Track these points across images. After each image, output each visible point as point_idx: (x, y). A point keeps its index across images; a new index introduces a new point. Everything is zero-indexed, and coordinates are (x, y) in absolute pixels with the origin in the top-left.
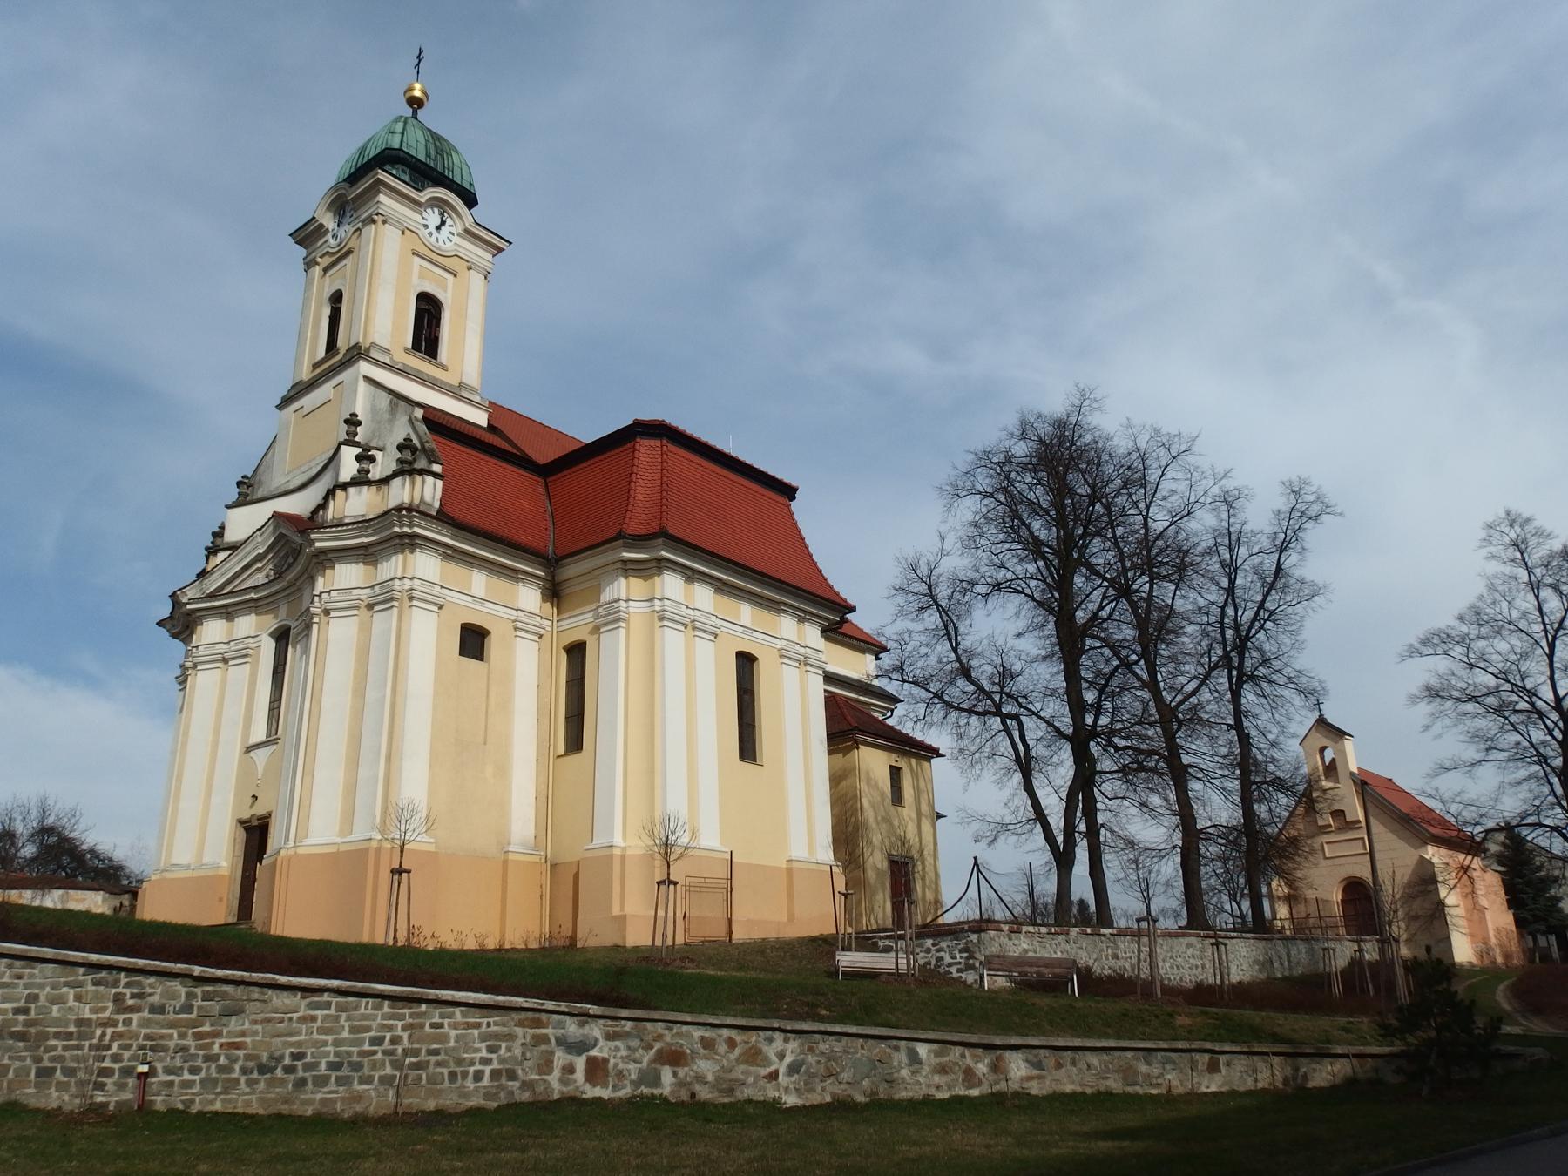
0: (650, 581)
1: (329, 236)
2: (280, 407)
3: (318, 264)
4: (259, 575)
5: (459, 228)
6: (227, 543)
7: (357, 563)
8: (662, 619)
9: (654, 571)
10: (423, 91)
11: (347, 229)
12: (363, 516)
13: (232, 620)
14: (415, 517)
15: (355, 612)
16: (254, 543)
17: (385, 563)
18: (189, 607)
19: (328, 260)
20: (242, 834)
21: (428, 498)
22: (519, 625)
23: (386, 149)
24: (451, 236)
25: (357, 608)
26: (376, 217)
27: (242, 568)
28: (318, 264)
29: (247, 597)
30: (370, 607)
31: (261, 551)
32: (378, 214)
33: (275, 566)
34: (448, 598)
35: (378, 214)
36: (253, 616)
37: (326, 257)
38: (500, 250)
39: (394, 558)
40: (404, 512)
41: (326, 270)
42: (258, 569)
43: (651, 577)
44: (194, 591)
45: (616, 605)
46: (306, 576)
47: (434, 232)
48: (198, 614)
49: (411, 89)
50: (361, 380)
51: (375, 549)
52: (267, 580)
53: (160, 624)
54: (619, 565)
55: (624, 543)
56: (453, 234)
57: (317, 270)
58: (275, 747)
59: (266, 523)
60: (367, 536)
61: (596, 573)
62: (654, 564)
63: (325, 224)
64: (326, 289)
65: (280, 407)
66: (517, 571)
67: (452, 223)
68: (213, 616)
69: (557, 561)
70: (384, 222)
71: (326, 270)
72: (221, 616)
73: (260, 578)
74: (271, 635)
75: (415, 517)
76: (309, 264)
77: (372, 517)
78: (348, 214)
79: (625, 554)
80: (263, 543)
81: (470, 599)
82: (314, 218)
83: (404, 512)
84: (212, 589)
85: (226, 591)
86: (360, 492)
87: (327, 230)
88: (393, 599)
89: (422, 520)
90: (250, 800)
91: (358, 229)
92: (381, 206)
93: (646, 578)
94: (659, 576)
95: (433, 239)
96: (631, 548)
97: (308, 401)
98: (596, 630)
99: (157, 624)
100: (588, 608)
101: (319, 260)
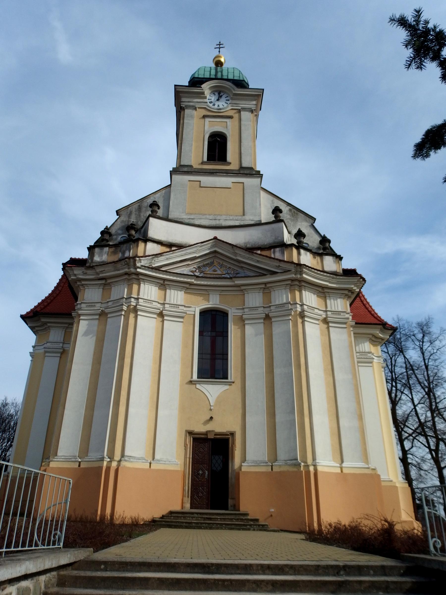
1: (207, 100)
16: (195, 249)
18: (138, 270)
20: (190, 441)
25: (318, 320)
34: (188, 313)
37: (203, 110)
41: (204, 117)
44: (146, 261)
60: (330, 282)
63: (205, 93)
72: (156, 284)
73: (185, 270)
87: (205, 98)
90: (209, 418)
95: (216, 106)
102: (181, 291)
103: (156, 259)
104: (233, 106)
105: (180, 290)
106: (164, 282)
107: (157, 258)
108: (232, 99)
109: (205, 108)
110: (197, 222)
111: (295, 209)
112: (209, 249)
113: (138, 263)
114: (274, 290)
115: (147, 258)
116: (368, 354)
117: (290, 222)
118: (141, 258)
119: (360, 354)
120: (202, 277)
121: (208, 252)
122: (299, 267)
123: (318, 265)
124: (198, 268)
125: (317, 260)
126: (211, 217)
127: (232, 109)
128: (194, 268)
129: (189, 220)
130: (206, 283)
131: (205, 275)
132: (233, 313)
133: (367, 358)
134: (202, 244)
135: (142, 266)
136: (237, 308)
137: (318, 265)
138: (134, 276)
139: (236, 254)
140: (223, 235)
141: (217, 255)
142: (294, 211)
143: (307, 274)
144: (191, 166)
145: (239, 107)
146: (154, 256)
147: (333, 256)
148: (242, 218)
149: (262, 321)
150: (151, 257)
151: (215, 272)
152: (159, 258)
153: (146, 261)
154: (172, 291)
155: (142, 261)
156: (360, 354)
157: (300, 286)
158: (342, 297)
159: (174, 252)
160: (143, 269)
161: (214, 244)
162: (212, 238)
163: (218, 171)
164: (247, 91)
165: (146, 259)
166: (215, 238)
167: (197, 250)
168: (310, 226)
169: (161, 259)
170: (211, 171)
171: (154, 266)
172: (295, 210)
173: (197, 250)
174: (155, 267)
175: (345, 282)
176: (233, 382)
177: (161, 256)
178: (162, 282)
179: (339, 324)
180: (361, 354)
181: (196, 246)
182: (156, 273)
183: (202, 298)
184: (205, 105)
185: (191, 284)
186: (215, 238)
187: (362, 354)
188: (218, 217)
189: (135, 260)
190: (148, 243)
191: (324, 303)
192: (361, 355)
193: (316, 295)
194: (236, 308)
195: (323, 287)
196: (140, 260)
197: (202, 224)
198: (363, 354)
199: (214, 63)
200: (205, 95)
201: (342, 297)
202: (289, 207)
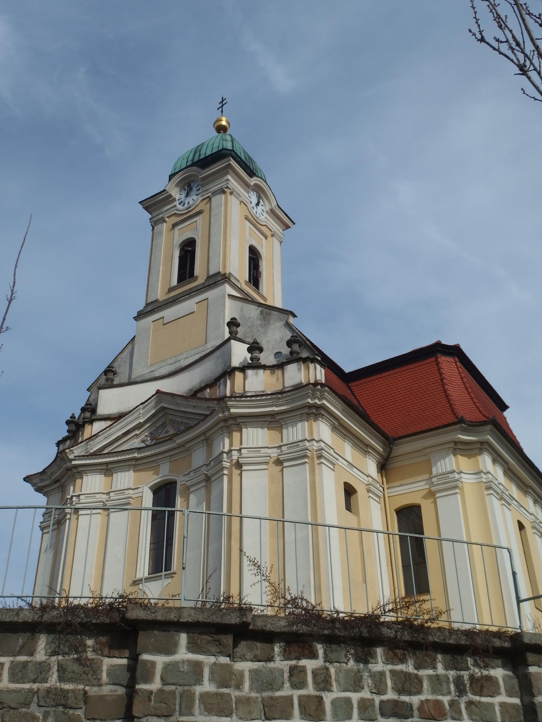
0: (473, 459)
1: (177, 203)
2: (137, 318)
3: (165, 222)
4: (136, 441)
5: (268, 208)
6: (100, 415)
7: (262, 428)
8: (488, 488)
9: (477, 451)
10: (228, 122)
11: (194, 199)
12: (263, 391)
13: (112, 475)
14: (326, 391)
15: (265, 467)
16: (137, 414)
17: (290, 429)
18: (74, 462)
19: (175, 219)
21: (318, 378)
22: (372, 488)
23: (223, 149)
24: (263, 212)
25: (267, 463)
26: (226, 190)
27: (123, 434)
28: (165, 222)
29: (131, 456)
30: (279, 462)
31: (142, 421)
32: (227, 187)
33: (151, 434)
35: (227, 187)
36: (132, 472)
37: (173, 217)
38: (288, 227)
39: (300, 425)
40: (319, 387)
41: (174, 226)
42: (136, 435)
43: (475, 455)
44: (80, 450)
45: (451, 476)
46: (203, 437)
47: (255, 207)
48: (80, 469)
49: (219, 120)
50: (227, 299)
51: (282, 417)
52: (143, 445)
53: (27, 479)
54: (452, 445)
55: (461, 427)
56: (264, 211)
57: (165, 227)
58: (170, 580)
59: (150, 399)
60: (277, 406)
61: (426, 451)
62: (479, 446)
63: (173, 194)
64: (176, 238)
65: (137, 318)
66: (368, 445)
67: (262, 204)
68: (93, 471)
69: (395, 439)
70: (231, 193)
71: (174, 226)
72: (100, 471)
73: (136, 443)
74: (151, 488)
75: (326, 391)
76: (155, 223)
77: (269, 393)
78: (195, 189)
79: (460, 436)
80: (144, 414)
81: (346, 463)
82: (165, 190)
83: (319, 387)
84: (94, 449)
85: (105, 452)
86: (257, 374)
87: (174, 200)
88: (305, 456)
89: (331, 396)
91: (209, 197)
92: (230, 183)
93: (469, 456)
94: (480, 455)
96: (464, 431)
97: (168, 313)
98: (431, 495)
99: (25, 479)
100: (419, 478)
101: (167, 219)
102: (128, 471)
103: (91, 442)
104: (203, 195)
105: (127, 469)
106: (107, 466)
107: (92, 442)
108: (203, 186)
109: (175, 214)
110: (157, 374)
111: (266, 308)
112: (155, 407)
113: (70, 455)
114: (287, 424)
115: (80, 445)
116: (449, 475)
117: (261, 329)
118: (72, 449)
119: (438, 479)
120: (154, 444)
121: (154, 411)
122: (221, 402)
123: (278, 382)
124: (150, 434)
125: (277, 375)
126: (172, 361)
127: (203, 200)
128: (146, 436)
129: (149, 374)
130: (143, 455)
131: (158, 441)
132: (181, 480)
133: (447, 483)
134: (144, 405)
135: (75, 457)
136: (184, 474)
137: (278, 382)
138: (74, 471)
139: (177, 404)
140: (166, 386)
141: (168, 412)
142: (266, 311)
143: (236, 407)
144: (156, 301)
145: (209, 193)
146: (88, 441)
147: (298, 362)
148: (203, 348)
149: (204, 484)
150: (84, 443)
151: (167, 433)
152: (95, 441)
153: (80, 449)
154: (119, 474)
155: (75, 451)
156: (438, 479)
157: (228, 427)
158: (304, 419)
159: (112, 426)
160: (78, 460)
161: (158, 399)
162: (154, 393)
163: (178, 297)
164: (213, 167)
165: (79, 447)
166: (158, 392)
167: (140, 414)
168: (284, 325)
169: (96, 442)
170: (172, 300)
171: (91, 451)
172: (267, 310)
173: (140, 414)
174: (94, 452)
175: (300, 396)
176: (175, 573)
177: (97, 437)
178: (105, 467)
179: (290, 461)
180: (438, 477)
181: (137, 411)
182: (94, 459)
183: (152, 472)
184: (175, 210)
185: (136, 459)
186: (158, 392)
187: (441, 477)
188: (180, 358)
189: (66, 453)
190: (94, 423)
191: (280, 435)
192: (440, 478)
193: (266, 428)
194: (182, 475)
195: (272, 415)
196: (71, 450)
197: (162, 374)
198: (443, 476)
199: (215, 128)
200: (173, 197)
201: (304, 419)
202: (261, 309)
